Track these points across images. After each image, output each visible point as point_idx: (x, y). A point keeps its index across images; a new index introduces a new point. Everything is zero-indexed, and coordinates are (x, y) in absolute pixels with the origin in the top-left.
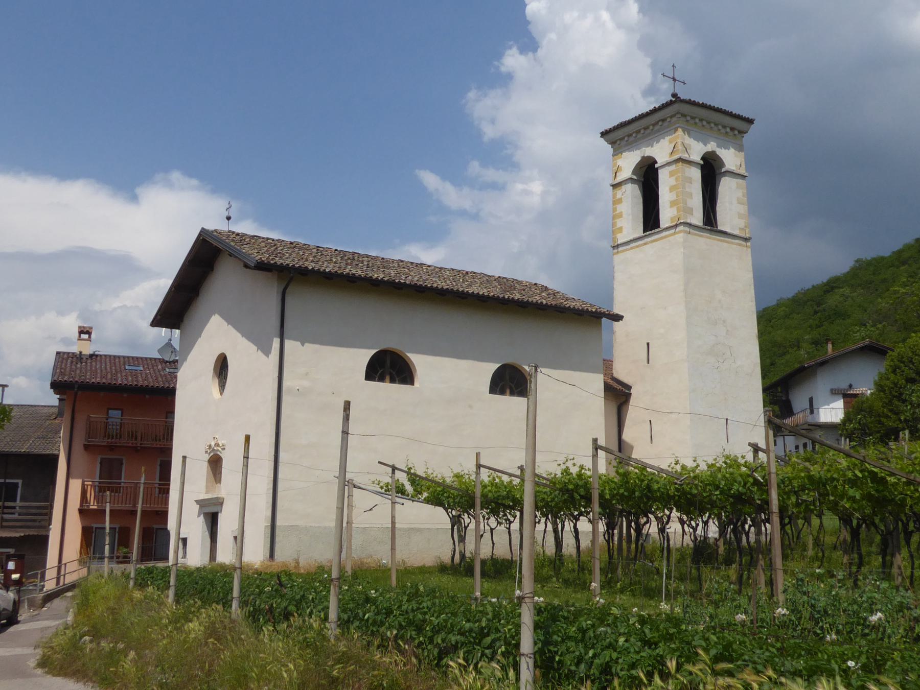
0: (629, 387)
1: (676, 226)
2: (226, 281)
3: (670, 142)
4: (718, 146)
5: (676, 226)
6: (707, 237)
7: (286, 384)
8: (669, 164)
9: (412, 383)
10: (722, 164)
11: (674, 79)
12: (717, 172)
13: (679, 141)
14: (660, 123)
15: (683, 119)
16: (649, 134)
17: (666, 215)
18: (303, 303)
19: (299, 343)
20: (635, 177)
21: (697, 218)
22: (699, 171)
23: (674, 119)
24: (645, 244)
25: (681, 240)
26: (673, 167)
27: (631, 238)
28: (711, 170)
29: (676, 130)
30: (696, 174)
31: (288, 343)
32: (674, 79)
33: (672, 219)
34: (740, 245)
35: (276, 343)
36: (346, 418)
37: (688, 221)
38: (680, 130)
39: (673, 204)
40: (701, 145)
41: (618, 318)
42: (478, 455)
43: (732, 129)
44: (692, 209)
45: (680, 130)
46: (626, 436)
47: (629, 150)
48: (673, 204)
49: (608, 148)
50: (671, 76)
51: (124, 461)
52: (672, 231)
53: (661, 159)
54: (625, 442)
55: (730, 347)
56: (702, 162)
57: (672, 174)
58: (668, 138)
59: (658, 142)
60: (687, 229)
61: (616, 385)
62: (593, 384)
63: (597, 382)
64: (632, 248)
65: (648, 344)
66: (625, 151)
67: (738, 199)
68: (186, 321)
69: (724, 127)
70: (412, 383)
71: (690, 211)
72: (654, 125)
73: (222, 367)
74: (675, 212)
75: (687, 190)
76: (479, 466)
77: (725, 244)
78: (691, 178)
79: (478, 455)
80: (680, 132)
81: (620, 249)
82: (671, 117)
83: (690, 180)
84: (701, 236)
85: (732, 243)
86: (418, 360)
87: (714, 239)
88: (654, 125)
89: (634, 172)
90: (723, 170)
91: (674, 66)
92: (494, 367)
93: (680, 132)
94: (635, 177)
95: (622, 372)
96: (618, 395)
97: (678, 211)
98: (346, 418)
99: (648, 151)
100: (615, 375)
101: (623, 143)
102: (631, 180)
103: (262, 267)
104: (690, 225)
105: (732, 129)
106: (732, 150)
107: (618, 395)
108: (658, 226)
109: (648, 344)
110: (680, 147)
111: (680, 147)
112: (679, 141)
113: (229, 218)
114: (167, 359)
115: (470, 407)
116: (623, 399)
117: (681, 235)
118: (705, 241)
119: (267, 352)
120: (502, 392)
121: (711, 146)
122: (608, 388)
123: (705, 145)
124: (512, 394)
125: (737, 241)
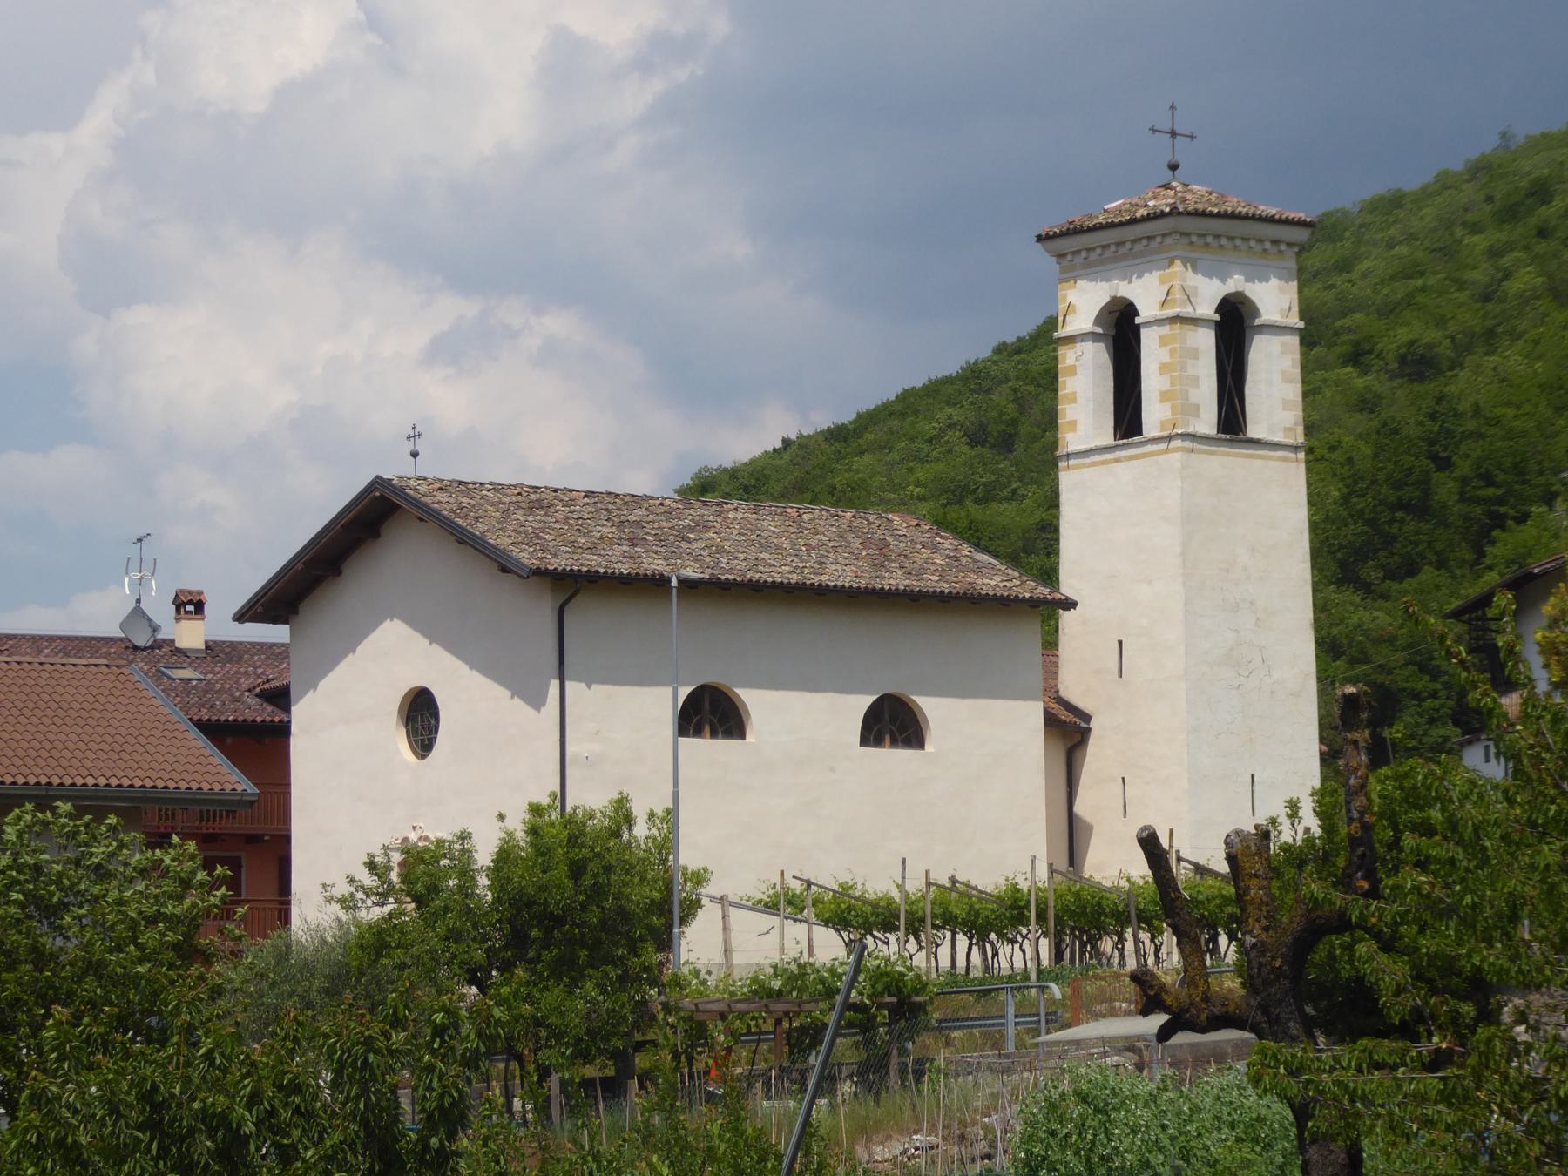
0: (1087, 718)
1: (1170, 438)
2: (401, 558)
3: (1162, 282)
4: (1249, 279)
5: (1170, 438)
6: (1224, 454)
7: (570, 750)
8: (1158, 322)
9: (742, 736)
10: (1255, 312)
11: (1173, 134)
12: (1247, 323)
13: (1177, 283)
14: (1145, 242)
15: (1185, 240)
16: (1125, 257)
17: (1154, 414)
18: (588, 620)
19: (583, 685)
20: (1099, 330)
21: (1207, 421)
22: (1213, 333)
23: (1168, 241)
24: (1117, 460)
25: (1178, 465)
26: (1165, 330)
27: (1092, 445)
28: (1234, 325)
29: (1171, 263)
30: (1206, 340)
31: (569, 685)
32: (1173, 134)
33: (1163, 425)
34: (1285, 459)
35: (554, 686)
36: (904, 869)
37: (1191, 430)
38: (1178, 262)
39: (1165, 396)
40: (1216, 282)
41: (1070, 604)
42: (927, 872)
43: (1275, 242)
44: (1197, 407)
45: (1178, 262)
46: (1077, 809)
47: (1091, 277)
48: (1165, 396)
49: (1051, 263)
50: (1168, 128)
51: (244, 863)
52: (1163, 446)
53: (1147, 310)
54: (1079, 818)
55: (1261, 649)
56: (1217, 317)
57: (1163, 341)
58: (1156, 274)
59: (1140, 276)
60: (1188, 444)
61: (1064, 715)
62: (1024, 720)
63: (1031, 714)
64: (1094, 464)
65: (1120, 643)
66: (1081, 277)
67: (1283, 373)
68: (306, 609)
69: (1260, 241)
70: (742, 736)
71: (1195, 411)
72: (1134, 241)
73: (420, 714)
74: (1169, 413)
75: (1190, 372)
76: (929, 884)
77: (1258, 462)
78: (1196, 350)
79: (927, 872)
80: (1178, 266)
81: (1072, 462)
82: (1164, 235)
83: (1194, 353)
84: (1213, 453)
85: (1270, 458)
86: (751, 699)
87: (1238, 456)
88: (1134, 241)
89: (1097, 321)
90: (1257, 322)
91: (1172, 108)
92: (866, 701)
93: (1178, 266)
94: (1099, 330)
95: (1073, 688)
96: (1068, 731)
97: (1173, 408)
98: (904, 869)
99: (1125, 290)
100: (1063, 694)
101: (1079, 260)
102: (1094, 337)
103: (539, 573)
104: (1193, 437)
105: (1275, 242)
106: (1274, 282)
107: (1068, 731)
108: (1140, 433)
109: (1120, 643)
110: (1177, 295)
111: (1177, 295)
112: (1177, 283)
113: (415, 455)
114: (141, 643)
115: (832, 769)
116: (1077, 738)
117: (1178, 455)
118: (1227, 463)
119: (537, 702)
120: (878, 742)
121: (1236, 283)
122: (1051, 721)
123: (1223, 281)
124: (894, 743)
125: (1279, 453)
